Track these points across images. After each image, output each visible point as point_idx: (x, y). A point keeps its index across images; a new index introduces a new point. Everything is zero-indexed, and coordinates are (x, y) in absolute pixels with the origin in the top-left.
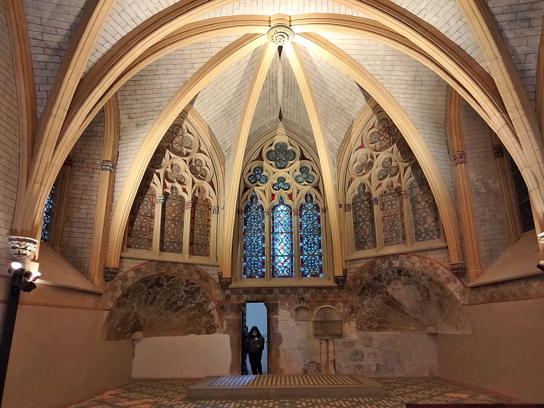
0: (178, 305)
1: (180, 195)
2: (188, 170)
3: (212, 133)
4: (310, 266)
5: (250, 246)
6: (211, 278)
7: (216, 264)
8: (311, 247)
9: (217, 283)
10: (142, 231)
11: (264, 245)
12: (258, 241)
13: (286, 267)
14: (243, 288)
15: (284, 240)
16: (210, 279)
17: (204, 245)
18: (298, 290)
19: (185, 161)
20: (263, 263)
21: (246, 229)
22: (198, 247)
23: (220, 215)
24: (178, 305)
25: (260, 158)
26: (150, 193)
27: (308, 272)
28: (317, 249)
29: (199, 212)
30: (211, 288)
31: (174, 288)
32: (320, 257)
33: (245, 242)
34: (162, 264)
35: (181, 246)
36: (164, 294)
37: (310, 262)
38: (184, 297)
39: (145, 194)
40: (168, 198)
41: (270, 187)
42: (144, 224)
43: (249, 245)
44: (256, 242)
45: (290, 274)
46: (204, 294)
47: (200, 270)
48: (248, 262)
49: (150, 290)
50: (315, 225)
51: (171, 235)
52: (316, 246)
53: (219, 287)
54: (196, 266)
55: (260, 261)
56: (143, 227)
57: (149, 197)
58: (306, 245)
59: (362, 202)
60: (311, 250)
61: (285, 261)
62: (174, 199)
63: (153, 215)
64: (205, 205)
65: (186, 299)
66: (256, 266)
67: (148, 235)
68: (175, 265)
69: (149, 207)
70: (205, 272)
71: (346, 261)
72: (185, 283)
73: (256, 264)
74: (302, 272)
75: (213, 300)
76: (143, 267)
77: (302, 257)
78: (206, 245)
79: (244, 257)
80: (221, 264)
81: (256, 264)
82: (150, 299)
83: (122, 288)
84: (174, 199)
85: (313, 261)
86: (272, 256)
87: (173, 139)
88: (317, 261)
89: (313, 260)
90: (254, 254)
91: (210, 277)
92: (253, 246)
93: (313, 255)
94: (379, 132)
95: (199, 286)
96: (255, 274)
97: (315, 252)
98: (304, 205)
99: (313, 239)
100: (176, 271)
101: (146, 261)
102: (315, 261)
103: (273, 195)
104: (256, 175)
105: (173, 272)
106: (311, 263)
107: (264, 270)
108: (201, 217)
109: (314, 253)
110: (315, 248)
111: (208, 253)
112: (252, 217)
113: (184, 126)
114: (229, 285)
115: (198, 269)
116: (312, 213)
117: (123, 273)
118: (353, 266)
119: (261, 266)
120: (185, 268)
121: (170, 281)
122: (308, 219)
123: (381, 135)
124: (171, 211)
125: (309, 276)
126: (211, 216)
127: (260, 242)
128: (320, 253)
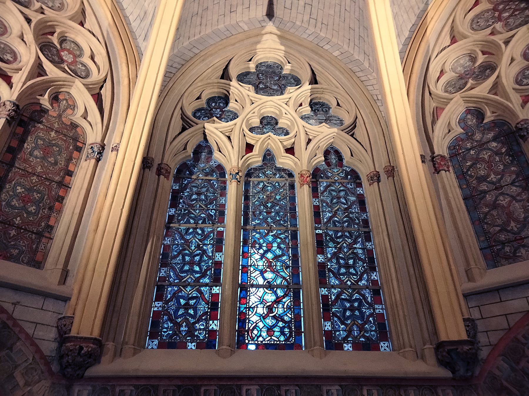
2: (29, 37)
4: (348, 318)
5: (180, 257)
7: (62, 290)
8: (347, 266)
9: (43, 357)
11: (218, 257)
12: (204, 245)
13: (278, 318)
14: (138, 378)
15: (275, 245)
16: (19, 339)
17: (33, 232)
18: (325, 389)
19: (29, 21)
20: (214, 305)
21: (174, 216)
25: (225, 75)
27: (343, 334)
28: (365, 272)
29: (40, 142)
32: (376, 293)
33: (167, 247)
37: (348, 305)
41: (244, 126)
43: (177, 256)
44: (198, 247)
45: (292, 340)
48: (170, 300)
50: (352, 213)
52: (361, 263)
55: (204, 299)
58: (334, 261)
59: (482, 146)
60: (348, 274)
61: (278, 300)
64: (65, 135)
66: (191, 312)
71: (466, 296)
73: (191, 307)
74: (328, 334)
77: (324, 291)
78: (40, 235)
79: (157, 286)
80: (76, 291)
81: (191, 307)
85: (356, 304)
86: (237, 331)
88: (367, 303)
89: (356, 300)
90: (189, 278)
91: (22, 330)
92: (187, 258)
93: (355, 288)
94: (495, 9)
96: (185, 337)
97: (361, 279)
98: (324, 172)
99: (350, 247)
102: (361, 304)
103: (249, 148)
104: (212, 109)
106: (352, 309)
107: (214, 325)
108: (44, 158)
109: (357, 282)
110: (360, 269)
111: (39, 257)
112: (195, 189)
114: (91, 365)
116: (342, 188)
118: (496, 309)
119: (205, 313)
122: (335, 201)
123: (501, 12)
125: (347, 347)
127: (209, 249)
128: (375, 282)
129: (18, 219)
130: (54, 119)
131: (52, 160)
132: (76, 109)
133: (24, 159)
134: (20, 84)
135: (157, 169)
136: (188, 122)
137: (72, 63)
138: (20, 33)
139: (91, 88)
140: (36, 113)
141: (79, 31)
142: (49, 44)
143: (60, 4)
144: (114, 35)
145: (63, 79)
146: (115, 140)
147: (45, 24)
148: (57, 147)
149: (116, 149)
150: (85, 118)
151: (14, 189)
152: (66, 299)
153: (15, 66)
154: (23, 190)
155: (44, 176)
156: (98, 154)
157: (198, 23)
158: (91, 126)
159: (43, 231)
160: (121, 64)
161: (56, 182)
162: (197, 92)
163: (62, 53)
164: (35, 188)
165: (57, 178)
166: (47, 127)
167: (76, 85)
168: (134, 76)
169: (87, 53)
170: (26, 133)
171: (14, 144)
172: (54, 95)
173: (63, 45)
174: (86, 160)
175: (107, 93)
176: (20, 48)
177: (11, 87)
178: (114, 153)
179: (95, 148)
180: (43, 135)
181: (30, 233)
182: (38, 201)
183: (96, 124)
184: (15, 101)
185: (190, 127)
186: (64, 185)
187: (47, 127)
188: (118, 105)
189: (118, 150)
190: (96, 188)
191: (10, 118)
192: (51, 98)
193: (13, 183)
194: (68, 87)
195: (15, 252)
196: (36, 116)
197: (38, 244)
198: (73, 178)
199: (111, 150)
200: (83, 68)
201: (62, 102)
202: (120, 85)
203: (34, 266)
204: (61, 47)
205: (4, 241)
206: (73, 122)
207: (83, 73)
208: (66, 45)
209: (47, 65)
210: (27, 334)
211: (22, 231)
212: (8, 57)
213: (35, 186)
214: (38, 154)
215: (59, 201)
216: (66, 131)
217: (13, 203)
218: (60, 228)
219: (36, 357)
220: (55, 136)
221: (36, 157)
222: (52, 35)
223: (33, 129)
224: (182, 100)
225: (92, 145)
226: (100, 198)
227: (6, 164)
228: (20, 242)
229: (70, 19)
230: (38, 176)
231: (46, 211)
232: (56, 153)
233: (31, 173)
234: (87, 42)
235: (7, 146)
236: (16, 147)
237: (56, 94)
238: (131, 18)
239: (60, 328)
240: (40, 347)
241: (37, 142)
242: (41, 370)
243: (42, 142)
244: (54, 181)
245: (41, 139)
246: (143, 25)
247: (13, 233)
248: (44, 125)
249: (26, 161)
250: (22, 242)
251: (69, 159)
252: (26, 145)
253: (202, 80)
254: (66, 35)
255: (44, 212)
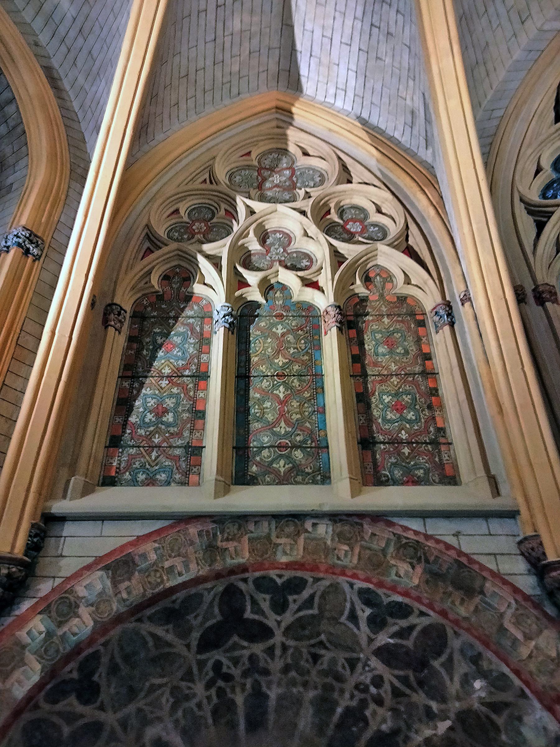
0: (373, 727)
1: (298, 303)
2: (313, 230)
3: (376, 128)
6: (485, 574)
9: (527, 598)
10: (162, 423)
16: (485, 578)
17: (426, 443)
19: (303, 213)
22: (399, 454)
23: (462, 327)
24: (373, 727)
26: (192, 313)
29: (378, 336)
30: (502, 625)
31: (323, 637)
34: (232, 529)
35: (324, 455)
36: (293, 674)
38: (387, 687)
39: (176, 318)
40: (257, 316)
42: (170, 403)
46: (476, 660)
47: (421, 539)
49: (217, 655)
51: (276, 423)
53: (546, 614)
54: (392, 524)
56: (166, 411)
57: (188, 324)
62: (280, 316)
63: (203, 369)
64: (399, 315)
65: (396, 693)
67: (186, 434)
68: (290, 529)
69: (191, 350)
70: (449, 547)
72: (364, 613)
75: (536, 693)
76: (149, 547)
78: (435, 443)
80: (521, 500)
82: (240, 699)
83: (46, 651)
84: (280, 316)
87: (264, 180)
91: (483, 567)
95: (434, 617)
100: (298, 554)
101: (166, 523)
105: (284, 559)
111: (449, 471)
113: (292, 148)
115: (410, 535)
117: (58, 581)
120: (341, 537)
121: (293, 607)
124: (269, 350)
126: (430, 343)
129: (403, 432)
130: (378, 303)
131: (400, 350)
132: (394, 280)
133: (373, 363)
134: (330, 283)
135: (535, 297)
136: (541, 212)
137: (362, 230)
138: (302, 232)
139: (398, 244)
140: (358, 307)
141: (352, 190)
142: (331, 225)
143: (319, 176)
144: (388, 168)
145: (364, 253)
146: (458, 289)
147: (318, 207)
148: (398, 332)
149: (466, 298)
150: (408, 284)
151: (381, 401)
152: (513, 514)
153: (314, 268)
154: (390, 397)
155: (403, 373)
156: (447, 317)
157: (484, 74)
158: (420, 288)
159: (436, 437)
160: (415, 195)
161: (418, 374)
162: (530, 167)
163: (348, 227)
164: (401, 390)
165: (418, 369)
166: (376, 316)
167: (381, 251)
168: (437, 198)
169: (371, 209)
170: (360, 333)
171: (356, 351)
172: (364, 277)
173: (344, 218)
174: (437, 332)
175: (417, 239)
176: (310, 247)
177: (323, 292)
178: (467, 305)
179: (441, 311)
180: (377, 327)
181: (424, 445)
182: (411, 404)
183: (426, 283)
184: (335, 303)
185: (549, 217)
186: (429, 374)
187: (376, 316)
188: (437, 245)
189: (470, 299)
190: (469, 360)
191: (339, 323)
192: (363, 281)
193: (377, 394)
194: (373, 258)
195: (420, 473)
196: (359, 310)
197: (439, 456)
198: (434, 361)
199: (460, 303)
200: (377, 229)
201: (376, 280)
202: (426, 220)
203: (449, 484)
204: (344, 221)
205: (404, 464)
206: (399, 295)
207: (379, 235)
208: (347, 216)
209: (343, 247)
210: (491, 571)
211: (414, 445)
212: (305, 263)
213: (399, 388)
214: (384, 350)
215: (434, 395)
216: (396, 309)
217: (389, 417)
218: (453, 428)
219: (517, 598)
220: (389, 321)
221: (384, 355)
222: (330, 214)
223: (364, 325)
224: (515, 189)
225: (435, 310)
226: (481, 369)
227: (360, 376)
228: (419, 459)
229: (337, 184)
230: (396, 375)
231: (427, 412)
232: (400, 340)
233: (388, 375)
234: (366, 197)
235: (350, 356)
236: (358, 353)
237: (365, 275)
238: (397, 135)
239: (526, 554)
240: (517, 585)
241: (375, 338)
242: (535, 615)
243: (380, 335)
244: (416, 374)
245: (378, 333)
246: (415, 132)
247: (406, 451)
248: (372, 315)
249: (376, 364)
250: (421, 459)
251: (418, 341)
252: (366, 346)
253: (530, 145)
254: (342, 204)
255: (425, 415)
